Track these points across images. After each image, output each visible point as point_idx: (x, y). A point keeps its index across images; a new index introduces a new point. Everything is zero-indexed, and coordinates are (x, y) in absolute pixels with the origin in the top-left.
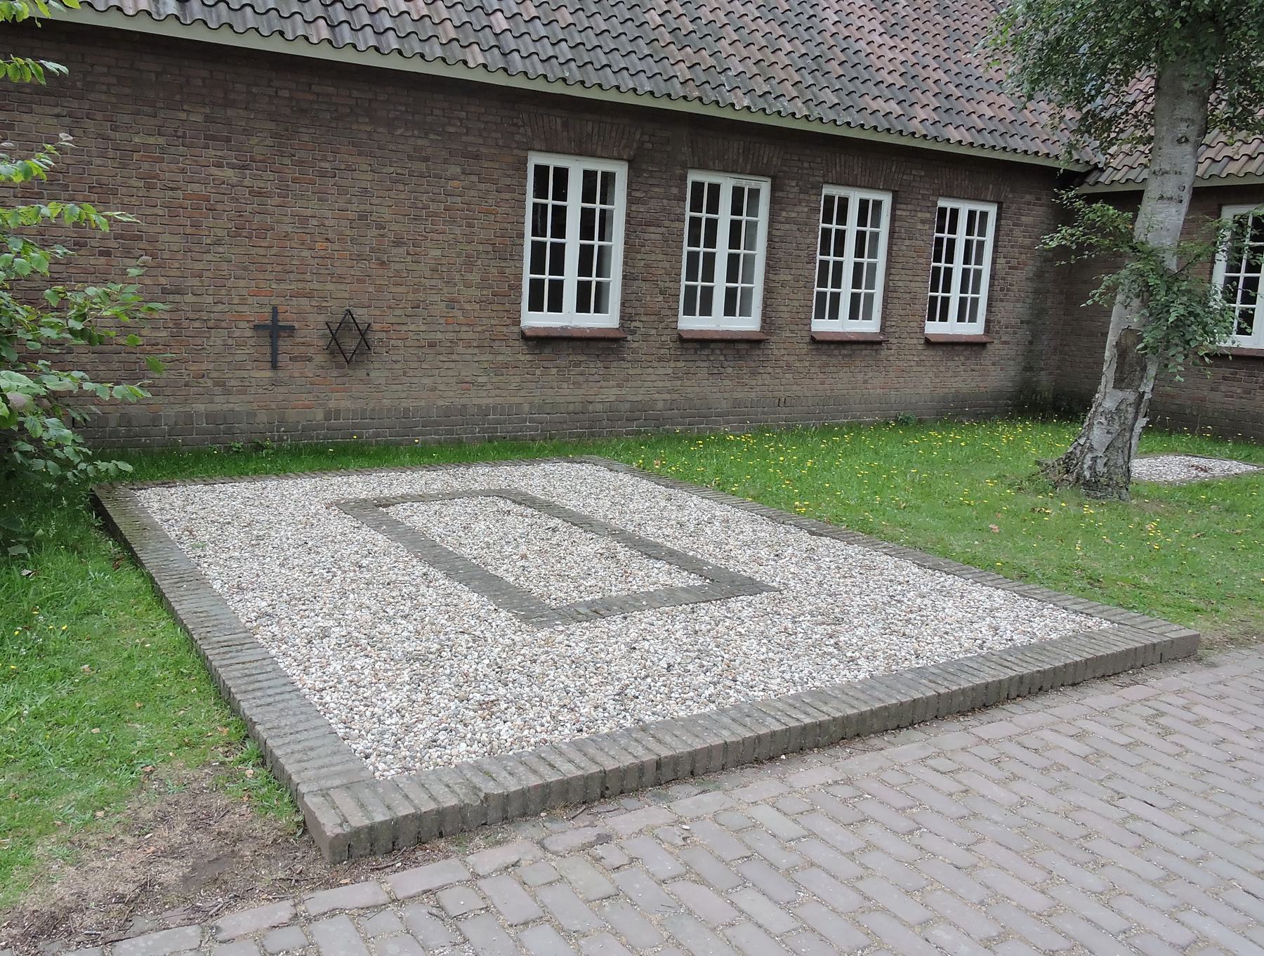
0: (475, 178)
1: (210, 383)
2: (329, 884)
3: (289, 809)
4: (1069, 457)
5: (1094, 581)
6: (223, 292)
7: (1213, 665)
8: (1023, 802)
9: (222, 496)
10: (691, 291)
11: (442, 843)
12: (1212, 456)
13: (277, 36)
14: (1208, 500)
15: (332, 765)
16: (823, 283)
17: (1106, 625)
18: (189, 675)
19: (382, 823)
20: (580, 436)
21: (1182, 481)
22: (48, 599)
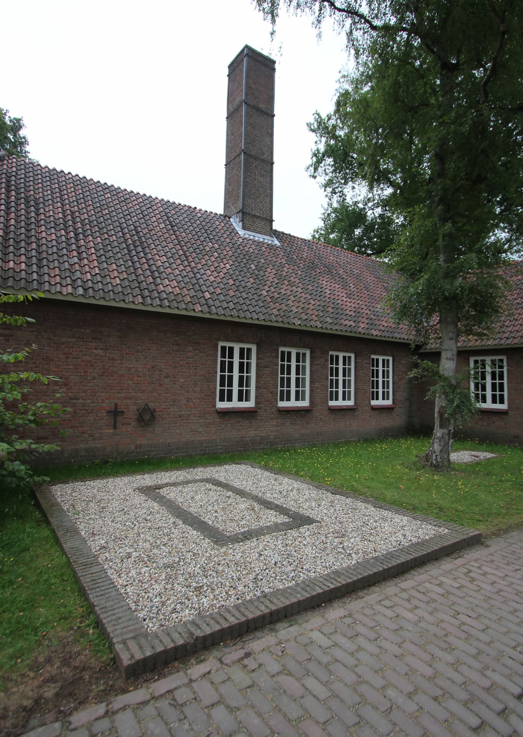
0: (198, 352)
1: (87, 436)
2: (124, 691)
3: (108, 651)
4: (427, 455)
5: (441, 509)
6: (95, 398)
7: (488, 546)
8: (421, 619)
9: (89, 487)
10: (282, 392)
11: (176, 664)
12: (478, 451)
13: (122, 302)
14: (479, 470)
15: (129, 626)
16: (332, 387)
17: (446, 531)
18: (67, 581)
19: (150, 656)
20: (240, 451)
21: (470, 462)
22: (6, 544)
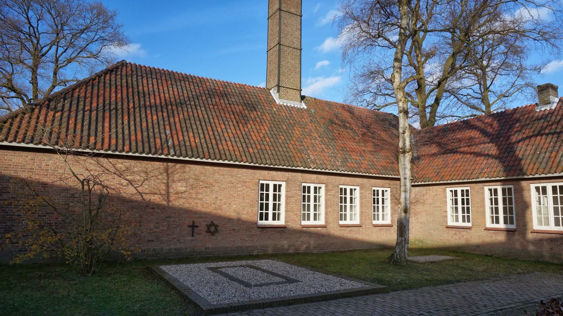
0: (245, 187)
